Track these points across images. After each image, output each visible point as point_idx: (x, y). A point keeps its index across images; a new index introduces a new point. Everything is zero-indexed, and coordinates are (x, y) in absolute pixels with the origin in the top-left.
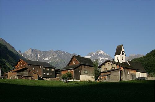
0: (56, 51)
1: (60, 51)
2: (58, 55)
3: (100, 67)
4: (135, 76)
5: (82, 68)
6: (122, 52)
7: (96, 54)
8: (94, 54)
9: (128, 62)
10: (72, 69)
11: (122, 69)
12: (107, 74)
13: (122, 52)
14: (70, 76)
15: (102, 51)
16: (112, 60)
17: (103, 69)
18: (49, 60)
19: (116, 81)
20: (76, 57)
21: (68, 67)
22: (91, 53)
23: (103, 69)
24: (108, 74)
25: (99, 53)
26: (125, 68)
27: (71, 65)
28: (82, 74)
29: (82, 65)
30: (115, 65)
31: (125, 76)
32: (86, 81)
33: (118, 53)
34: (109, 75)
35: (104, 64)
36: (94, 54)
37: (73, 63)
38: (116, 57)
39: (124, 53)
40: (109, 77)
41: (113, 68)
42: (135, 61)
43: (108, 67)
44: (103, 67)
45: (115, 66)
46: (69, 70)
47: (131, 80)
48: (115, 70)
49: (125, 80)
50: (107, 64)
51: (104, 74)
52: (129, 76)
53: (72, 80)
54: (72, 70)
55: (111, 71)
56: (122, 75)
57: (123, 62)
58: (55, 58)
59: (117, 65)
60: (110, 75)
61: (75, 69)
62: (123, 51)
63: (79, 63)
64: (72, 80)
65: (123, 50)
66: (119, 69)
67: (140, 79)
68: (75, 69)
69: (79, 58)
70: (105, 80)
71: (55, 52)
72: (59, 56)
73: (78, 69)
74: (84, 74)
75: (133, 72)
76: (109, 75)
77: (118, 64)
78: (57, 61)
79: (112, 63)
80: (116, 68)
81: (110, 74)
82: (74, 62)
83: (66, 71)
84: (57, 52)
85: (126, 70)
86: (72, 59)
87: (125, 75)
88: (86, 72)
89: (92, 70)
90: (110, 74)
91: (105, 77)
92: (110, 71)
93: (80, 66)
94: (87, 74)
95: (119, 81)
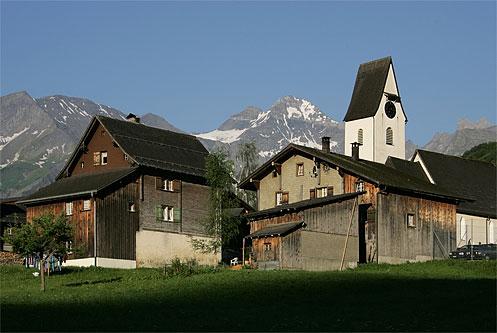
0: (47, 99)
1: (68, 100)
2: (58, 125)
3: (252, 186)
4: (448, 235)
5: (145, 187)
6: (384, 100)
7: (271, 118)
8: (260, 116)
9: (418, 159)
10: (87, 197)
11: (370, 194)
12: (286, 222)
13: (384, 100)
14: (61, 239)
15: (305, 103)
16: (320, 147)
17: (267, 197)
18: (20, 158)
19: (338, 266)
20: (113, 124)
21: (68, 184)
22: (244, 114)
23: (267, 197)
24: (292, 223)
25: (291, 111)
26: (388, 190)
27: (81, 171)
28: (144, 223)
29: (142, 171)
30: (334, 173)
31: (387, 234)
32: (169, 264)
33: (362, 107)
34: (291, 230)
35: (273, 168)
36: (260, 116)
37: (97, 159)
38: (352, 129)
39: (397, 105)
40: (296, 243)
41: (323, 194)
42: (482, 159)
43: (297, 183)
44: (268, 184)
45: (334, 182)
46: (68, 200)
47: (423, 259)
48: (332, 200)
49: (389, 260)
50: (289, 167)
51: (272, 224)
52: (415, 236)
53: (87, 262)
54: (87, 204)
55: (314, 205)
56: (374, 229)
57: (392, 160)
58: (42, 142)
59: (343, 172)
60: (303, 233)
61: (100, 195)
62: (391, 97)
63: (128, 162)
64: (87, 262)
65: (390, 87)
66: (355, 195)
67: (477, 257)
68: (100, 195)
69: (130, 133)
70: (274, 260)
71: (39, 103)
72: (65, 128)
73: (125, 196)
74: (159, 225)
75: (440, 215)
76: (291, 230)
77: (353, 167)
78: (52, 157)
79: (318, 161)
80: (338, 191)
81: (299, 226)
82: (99, 158)
83: (54, 210)
84: (51, 105)
85: (396, 204)
86: (88, 138)
87: (392, 228)
88: (170, 215)
89: (201, 198)
90: (299, 226)
91: (273, 242)
92: (302, 207)
93: (131, 178)
94: (177, 226)
95: (353, 265)
